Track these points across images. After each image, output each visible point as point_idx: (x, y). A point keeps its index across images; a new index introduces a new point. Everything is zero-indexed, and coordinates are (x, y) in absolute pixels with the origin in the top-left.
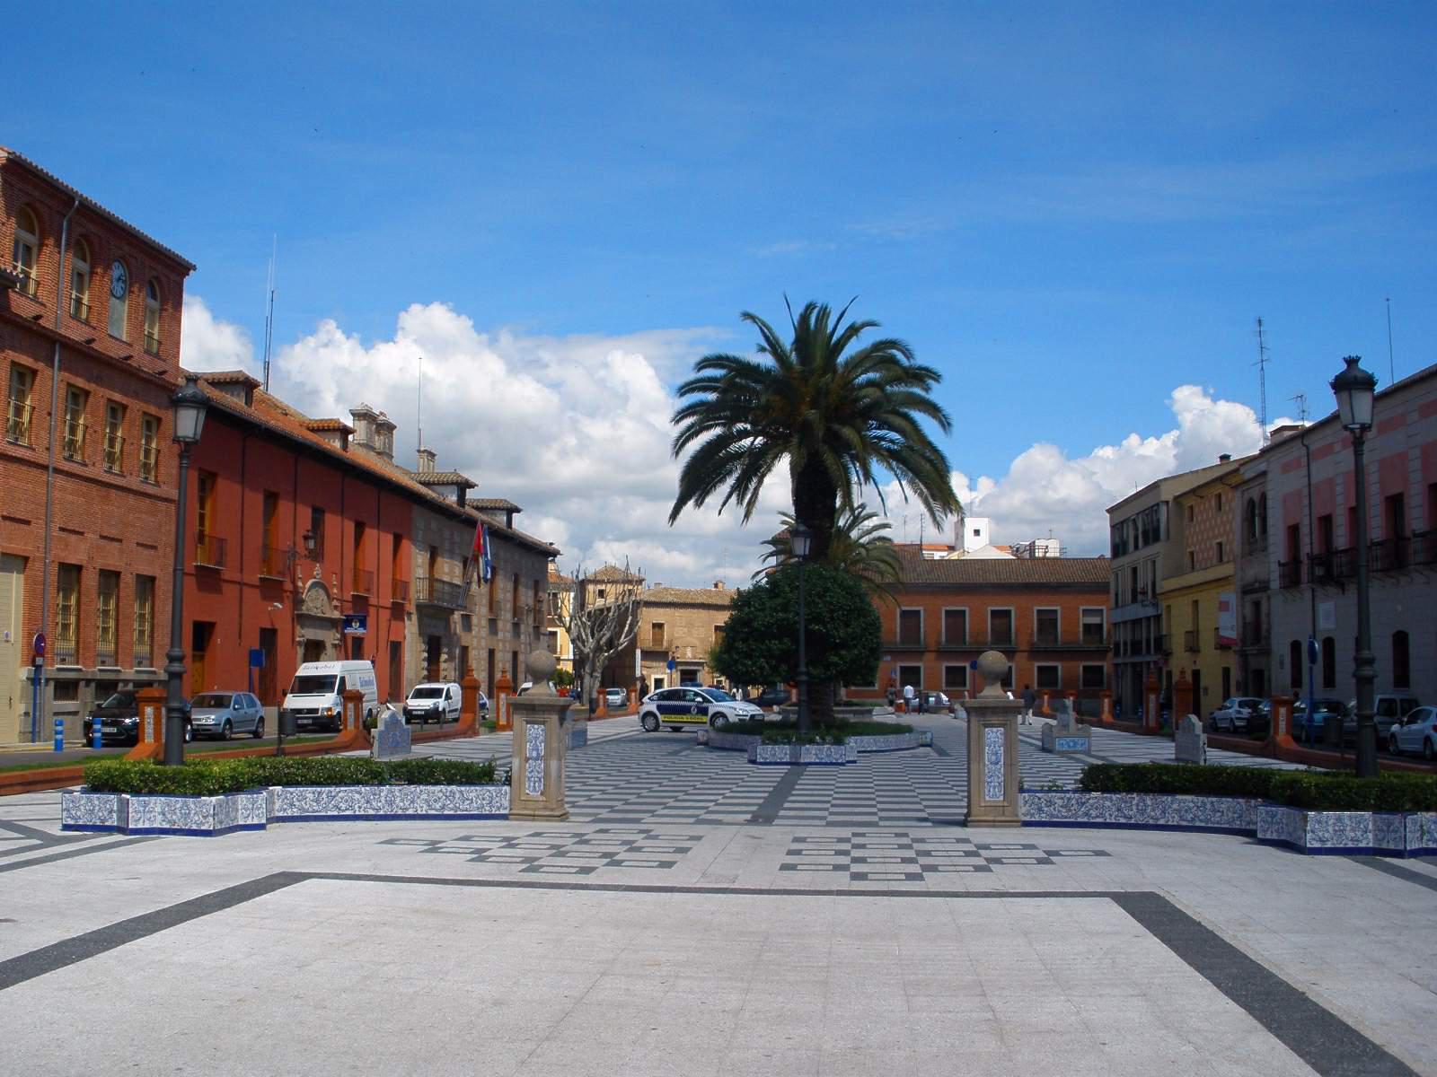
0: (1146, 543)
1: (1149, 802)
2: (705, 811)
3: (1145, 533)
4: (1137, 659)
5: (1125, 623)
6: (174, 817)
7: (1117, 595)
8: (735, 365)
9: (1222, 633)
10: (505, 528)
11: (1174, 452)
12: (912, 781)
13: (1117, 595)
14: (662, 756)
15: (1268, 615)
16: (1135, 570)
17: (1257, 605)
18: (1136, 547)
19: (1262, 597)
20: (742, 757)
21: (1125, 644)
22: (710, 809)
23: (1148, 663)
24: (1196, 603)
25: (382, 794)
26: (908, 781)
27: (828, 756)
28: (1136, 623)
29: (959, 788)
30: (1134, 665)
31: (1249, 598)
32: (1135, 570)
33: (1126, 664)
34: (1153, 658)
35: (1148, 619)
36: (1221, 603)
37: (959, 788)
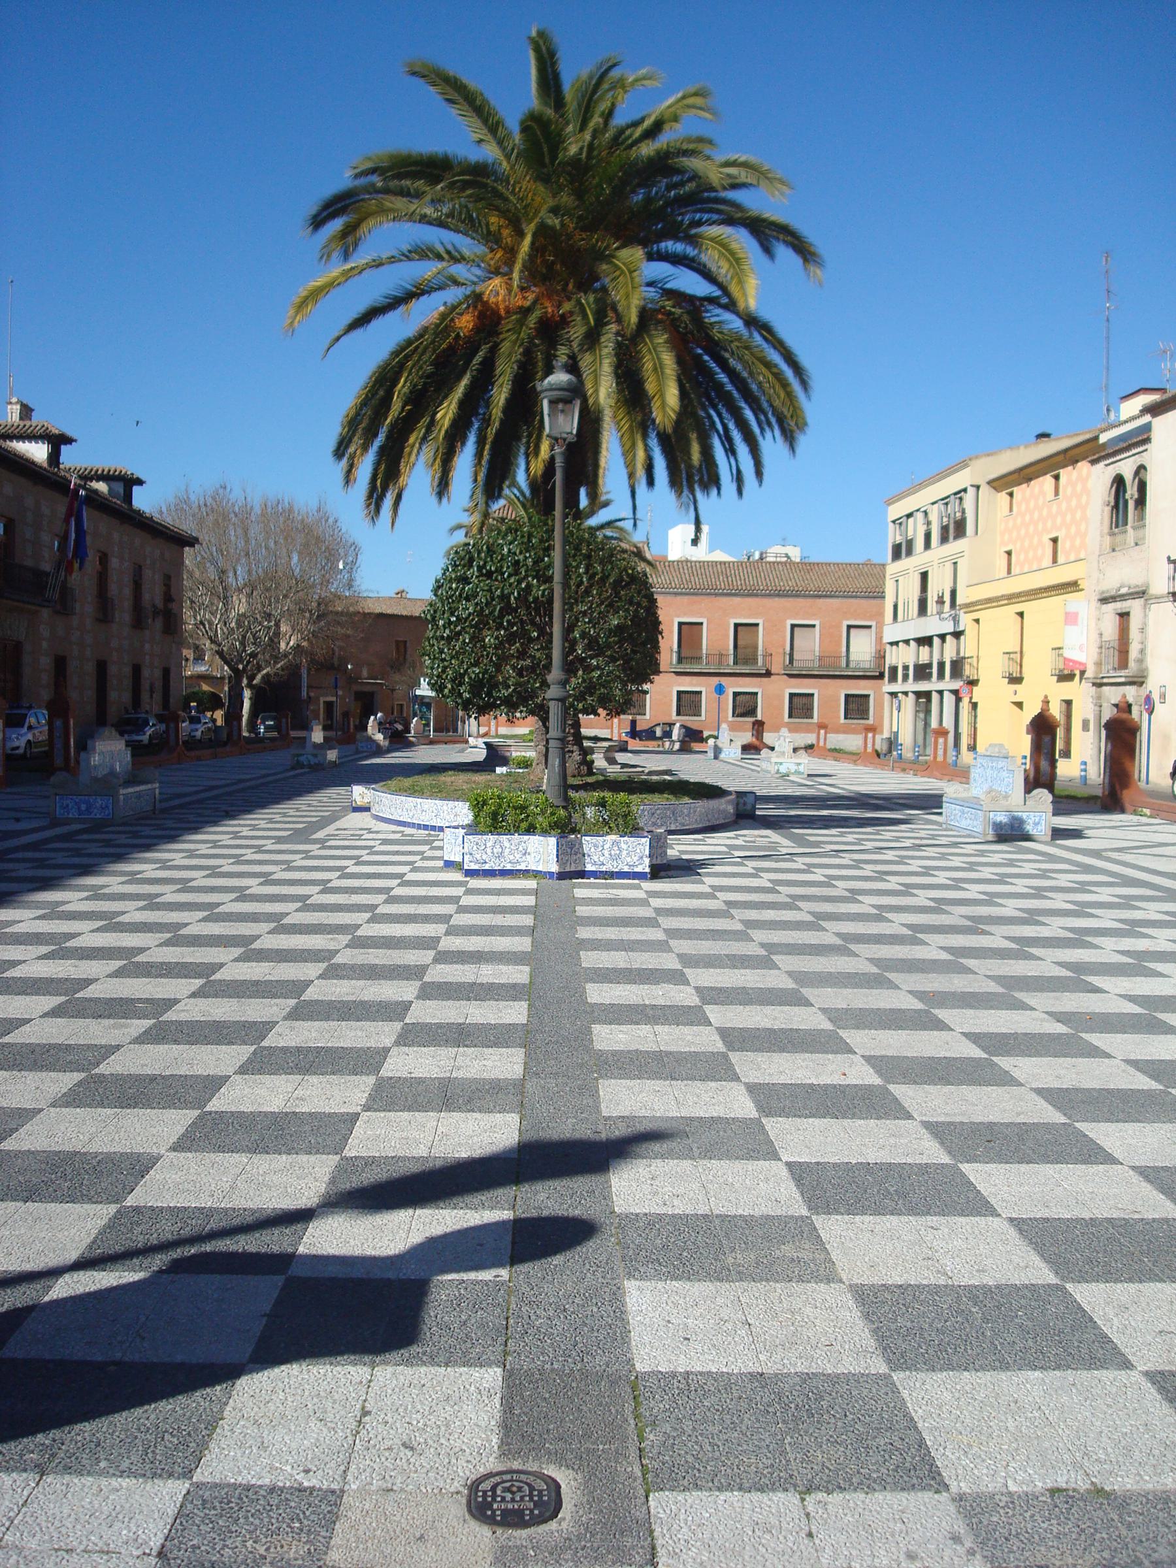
0: (944, 539)
1: (507, 844)
2: (257, 945)
3: (945, 530)
4: (923, 686)
5: (907, 642)
6: (484, 857)
7: (896, 607)
8: (383, 466)
9: (1067, 654)
10: (45, 465)
11: (594, 756)
12: (656, 902)
13: (896, 607)
14: (279, 840)
15: (1142, 630)
16: (924, 576)
17: (1124, 616)
18: (927, 545)
19: (1135, 607)
20: (595, 864)
21: (906, 668)
22: (348, 870)
23: (941, 692)
24: (1021, 614)
25: (605, 847)
26: (661, 947)
27: (500, 856)
28: (926, 641)
29: (753, 915)
30: (918, 694)
31: (1111, 607)
32: (924, 576)
33: (906, 693)
34: (948, 684)
35: (942, 637)
36: (1067, 614)
37: (753, 915)
